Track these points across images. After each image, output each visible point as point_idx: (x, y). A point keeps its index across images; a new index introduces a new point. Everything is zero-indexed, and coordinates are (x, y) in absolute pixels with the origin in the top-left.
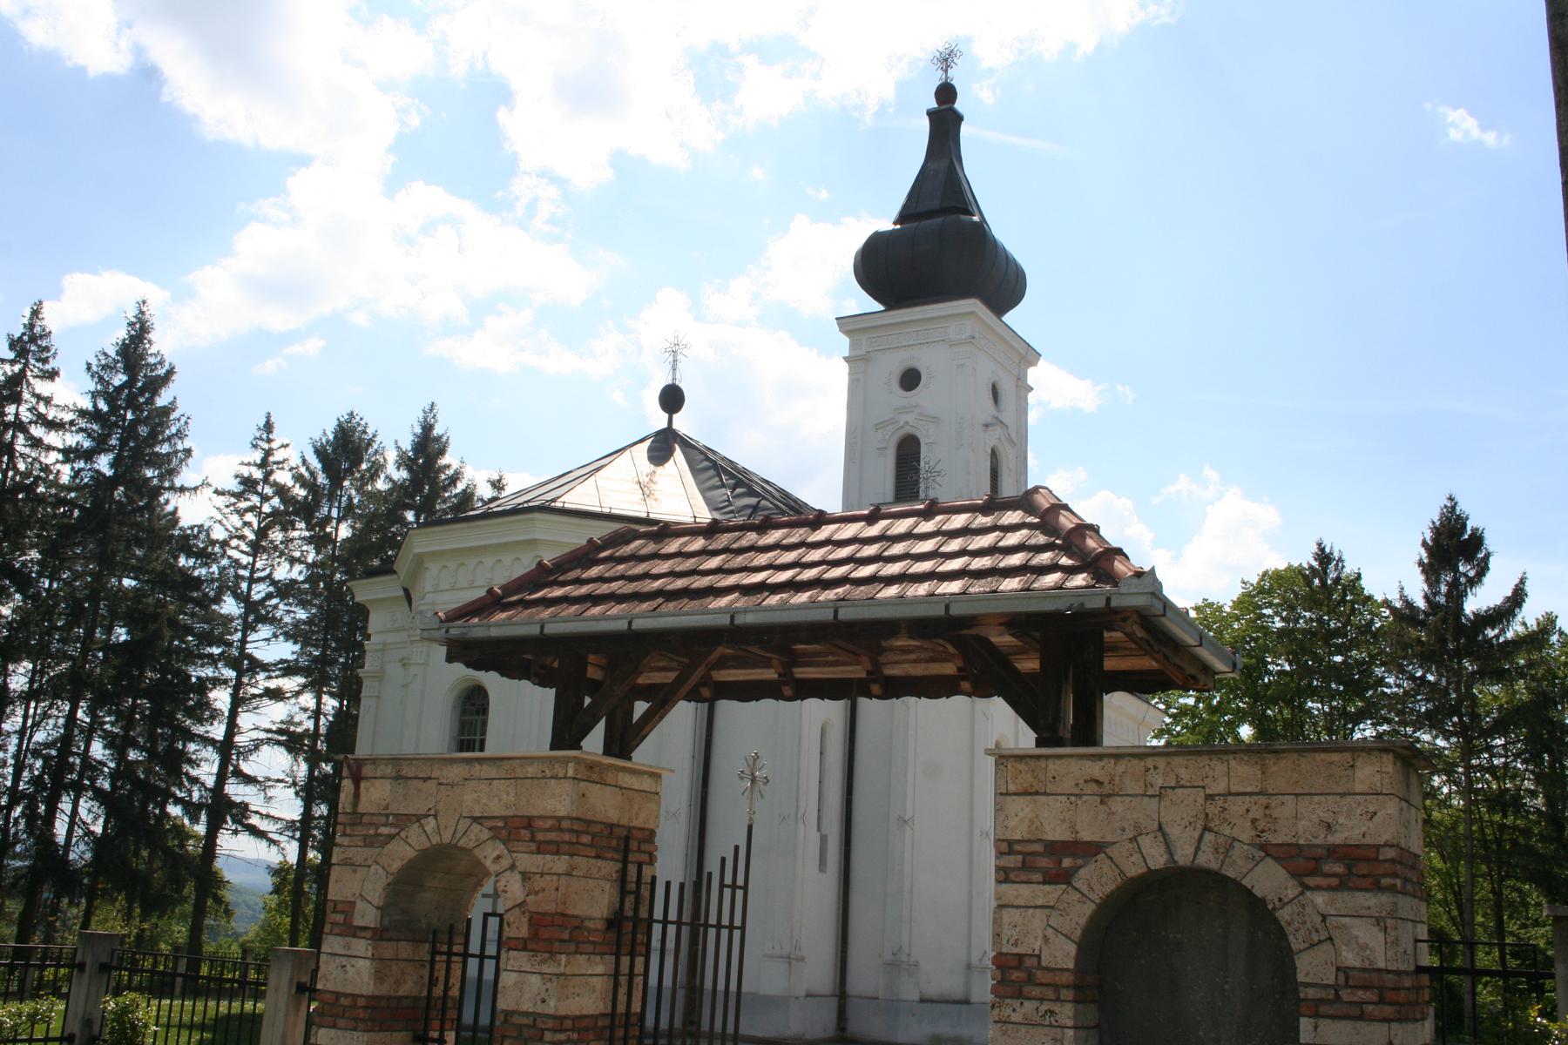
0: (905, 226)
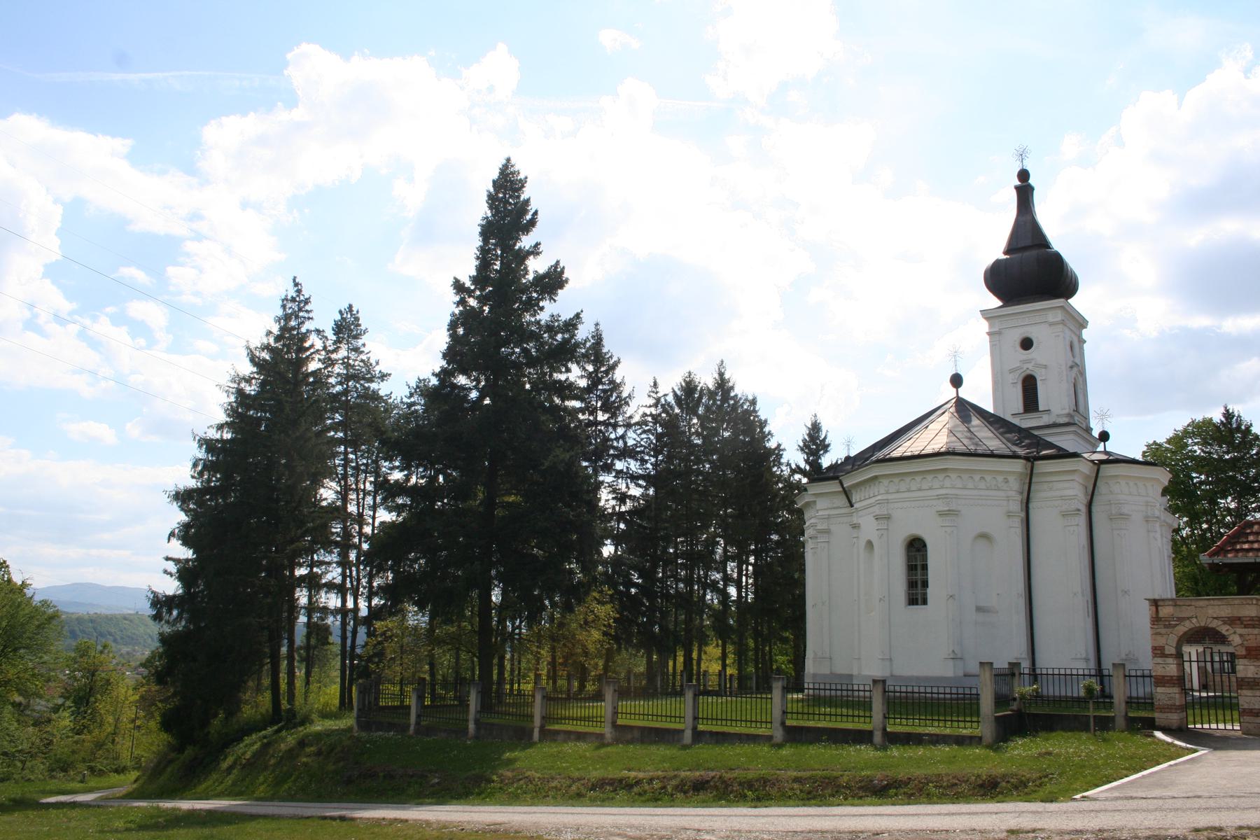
0: (1014, 256)
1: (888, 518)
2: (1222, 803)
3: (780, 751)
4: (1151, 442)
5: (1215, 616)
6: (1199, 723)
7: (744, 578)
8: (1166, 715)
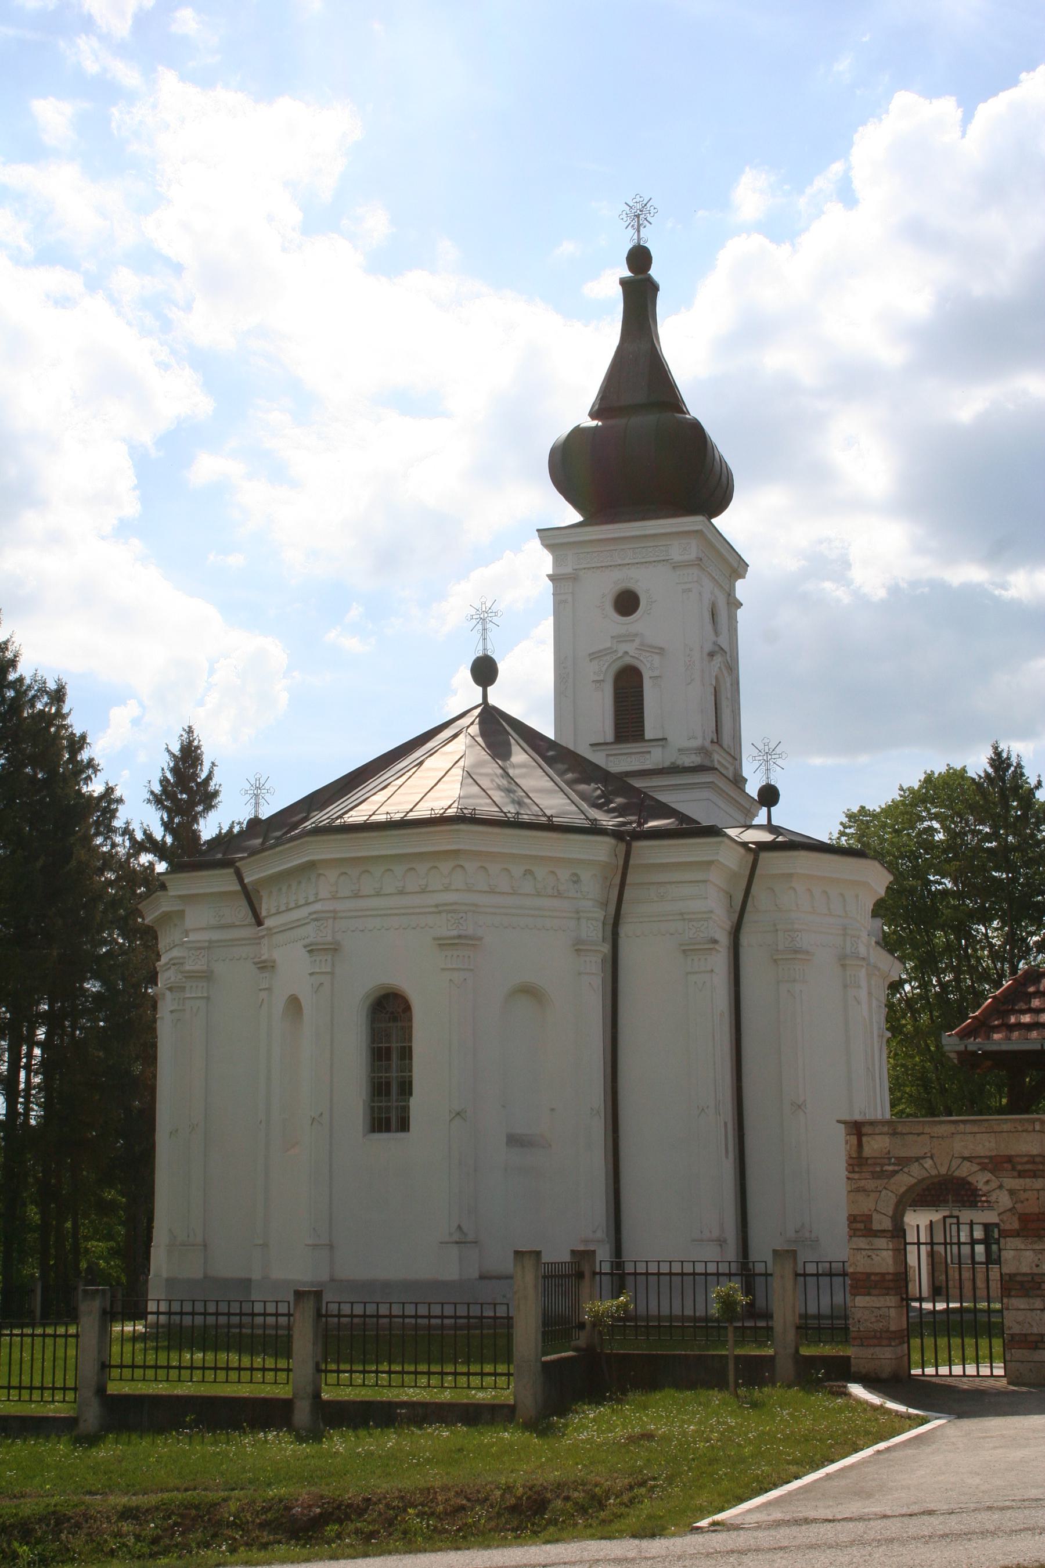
0: (611, 422)
1: (334, 949)
2: (973, 1522)
3: (94, 1451)
4: (855, 809)
5: (967, 1154)
6: (931, 1365)
7: (23, 1074)
8: (871, 1350)
